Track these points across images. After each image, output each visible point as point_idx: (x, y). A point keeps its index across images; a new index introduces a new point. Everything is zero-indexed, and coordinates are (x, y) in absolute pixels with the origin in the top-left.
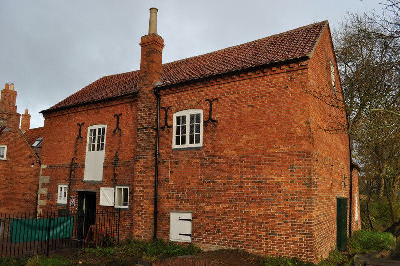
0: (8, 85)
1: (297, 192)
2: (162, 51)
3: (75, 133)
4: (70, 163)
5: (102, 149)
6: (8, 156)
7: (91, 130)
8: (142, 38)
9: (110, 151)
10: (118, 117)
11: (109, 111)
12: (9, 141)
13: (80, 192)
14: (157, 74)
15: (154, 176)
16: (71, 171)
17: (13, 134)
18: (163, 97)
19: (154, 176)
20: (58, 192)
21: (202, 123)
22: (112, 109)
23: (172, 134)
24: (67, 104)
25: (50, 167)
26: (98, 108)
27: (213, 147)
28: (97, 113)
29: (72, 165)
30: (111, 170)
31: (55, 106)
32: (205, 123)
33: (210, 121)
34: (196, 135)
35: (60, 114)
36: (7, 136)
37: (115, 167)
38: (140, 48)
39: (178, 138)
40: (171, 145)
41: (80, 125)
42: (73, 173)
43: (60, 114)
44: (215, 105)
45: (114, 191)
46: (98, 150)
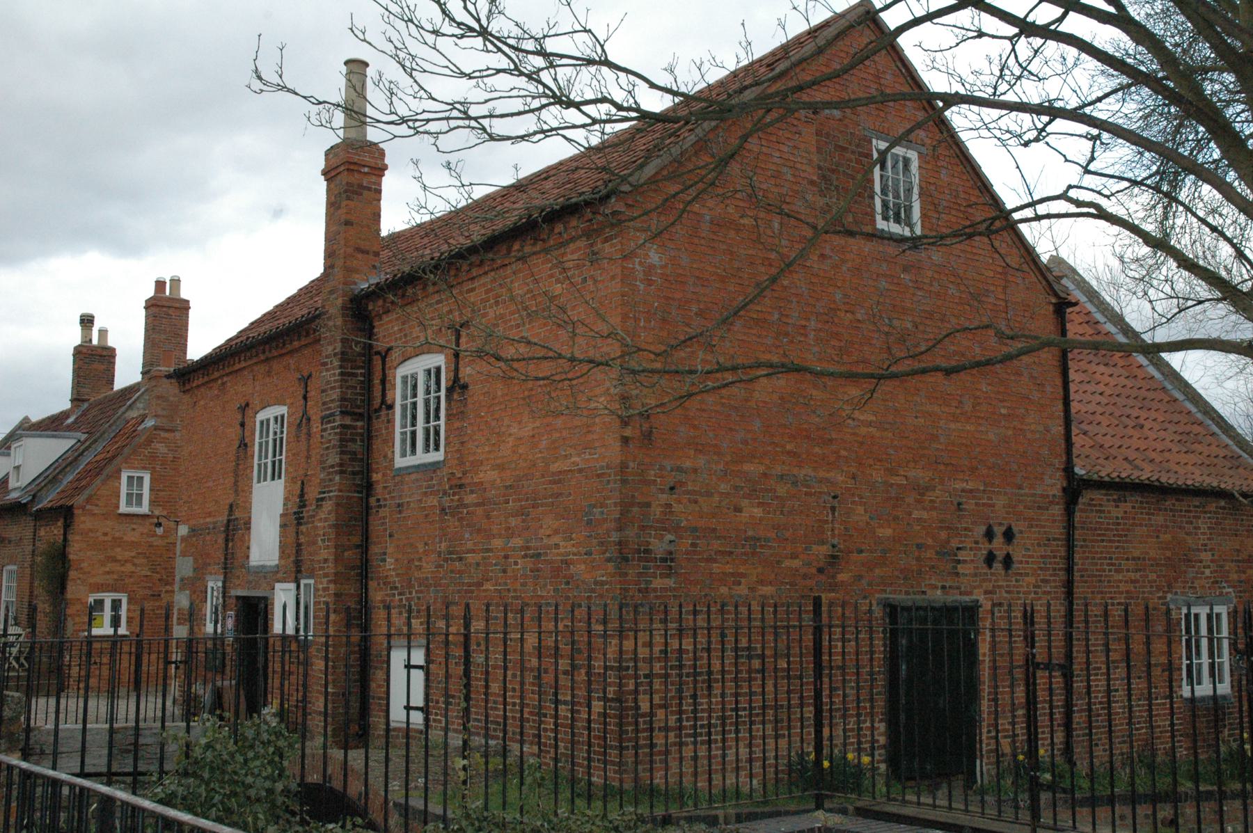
0: (160, 285)
1: (596, 583)
2: (380, 184)
3: (233, 433)
4: (223, 519)
5: (280, 477)
6: (152, 503)
7: (405, 379)
8: (327, 153)
9: (291, 480)
10: (306, 380)
11: (287, 367)
12: (153, 457)
13: (244, 598)
14: (360, 256)
15: (357, 547)
16: (227, 540)
17: (163, 434)
18: (376, 324)
19: (357, 547)
20: (206, 601)
21: (443, 393)
22: (292, 361)
23: (394, 426)
24: (284, 321)
25: (193, 530)
26: (267, 359)
27: (461, 462)
28: (269, 374)
29: (229, 521)
30: (291, 530)
31: (237, 337)
32: (450, 391)
33: (457, 386)
34: (406, 427)
35: (206, 379)
36: (149, 442)
37: (299, 524)
38: (323, 184)
39: (129, 495)
40: (392, 460)
41: (244, 408)
42: (230, 545)
43: (206, 379)
44: (464, 333)
45: (294, 592)
46: (273, 479)
